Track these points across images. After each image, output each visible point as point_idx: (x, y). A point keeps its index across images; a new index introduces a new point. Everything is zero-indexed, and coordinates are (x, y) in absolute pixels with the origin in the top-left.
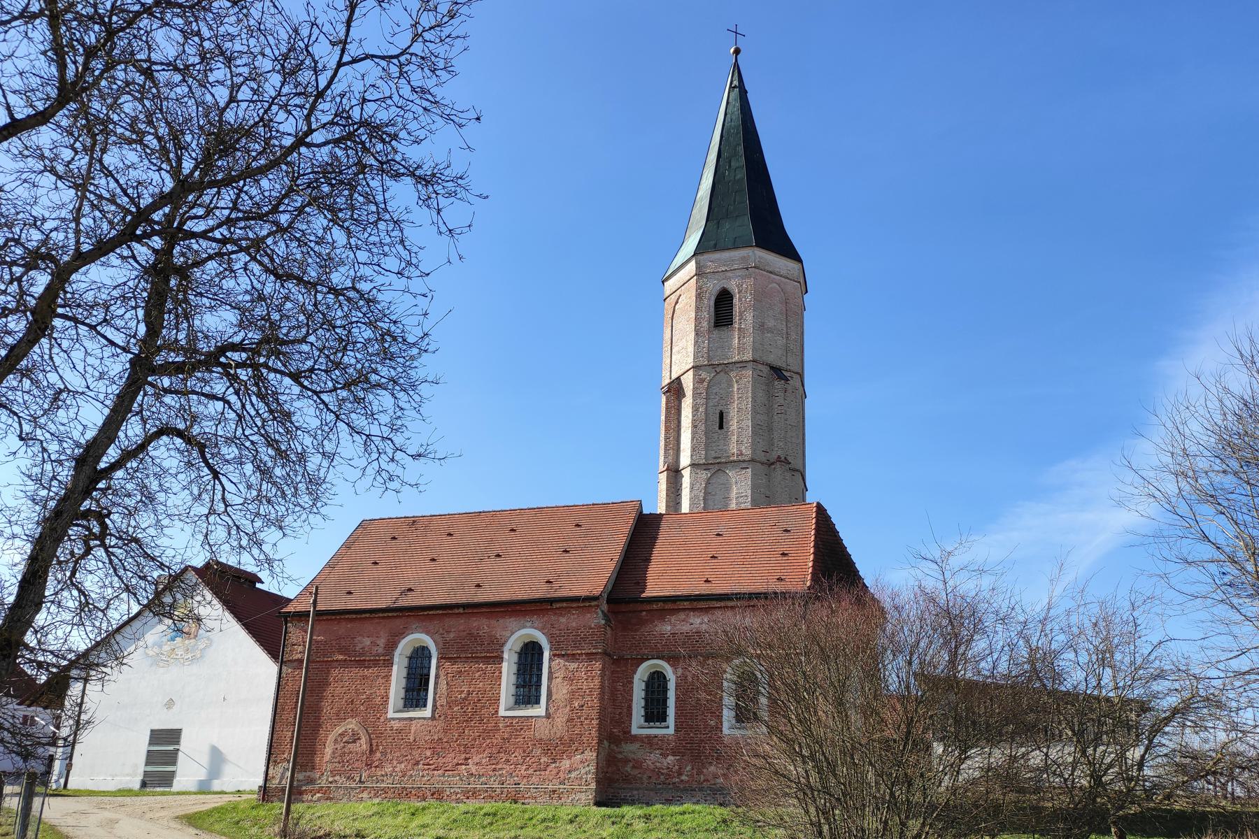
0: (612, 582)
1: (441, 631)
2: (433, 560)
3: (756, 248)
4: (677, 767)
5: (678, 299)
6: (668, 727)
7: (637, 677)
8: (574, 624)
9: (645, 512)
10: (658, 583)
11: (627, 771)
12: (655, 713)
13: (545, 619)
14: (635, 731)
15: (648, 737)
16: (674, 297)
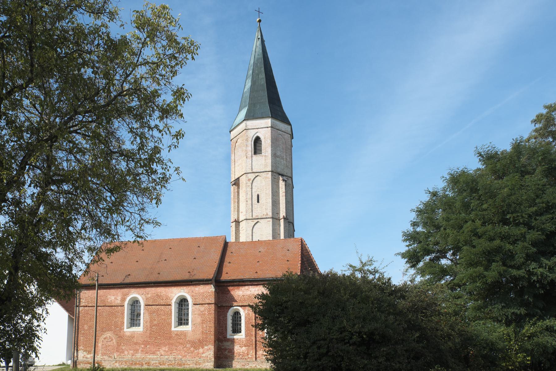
4: (247, 352)
8: (202, 291)
11: (226, 354)
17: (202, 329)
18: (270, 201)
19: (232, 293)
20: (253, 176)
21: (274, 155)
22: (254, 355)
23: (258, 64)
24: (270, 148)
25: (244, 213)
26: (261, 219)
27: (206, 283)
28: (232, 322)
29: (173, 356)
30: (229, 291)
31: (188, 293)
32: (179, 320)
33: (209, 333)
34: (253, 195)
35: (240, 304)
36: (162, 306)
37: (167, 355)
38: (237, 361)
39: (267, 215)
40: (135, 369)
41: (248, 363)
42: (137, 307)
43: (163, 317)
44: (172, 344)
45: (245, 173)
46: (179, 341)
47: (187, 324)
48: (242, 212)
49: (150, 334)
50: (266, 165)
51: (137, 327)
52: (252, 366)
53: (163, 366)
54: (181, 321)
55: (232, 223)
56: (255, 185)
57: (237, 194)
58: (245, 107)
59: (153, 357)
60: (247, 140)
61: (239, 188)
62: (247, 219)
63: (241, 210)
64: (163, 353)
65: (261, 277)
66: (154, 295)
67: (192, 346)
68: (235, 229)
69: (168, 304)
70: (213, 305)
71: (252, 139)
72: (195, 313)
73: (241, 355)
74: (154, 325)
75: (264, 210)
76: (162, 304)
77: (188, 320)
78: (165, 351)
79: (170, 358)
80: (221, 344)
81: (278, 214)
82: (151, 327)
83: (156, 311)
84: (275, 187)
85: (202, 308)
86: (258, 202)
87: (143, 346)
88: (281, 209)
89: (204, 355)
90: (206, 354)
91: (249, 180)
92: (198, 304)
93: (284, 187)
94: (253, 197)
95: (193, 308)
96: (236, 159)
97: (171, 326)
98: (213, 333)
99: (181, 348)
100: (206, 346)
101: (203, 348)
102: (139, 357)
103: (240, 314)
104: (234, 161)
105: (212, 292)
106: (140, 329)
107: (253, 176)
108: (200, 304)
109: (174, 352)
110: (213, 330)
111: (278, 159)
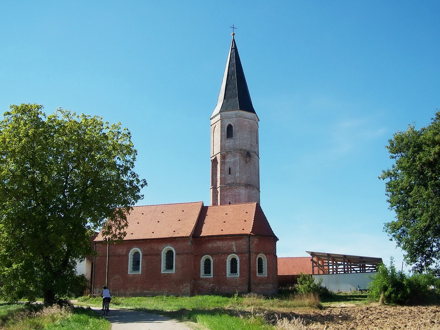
0: (194, 231)
1: (143, 247)
3: (240, 111)
5: (215, 126)
6: (211, 275)
7: (202, 260)
9: (204, 206)
10: (205, 232)
12: (207, 271)
14: (201, 277)
15: (206, 278)
16: (214, 126)
101: (182, 285)
102: (138, 292)
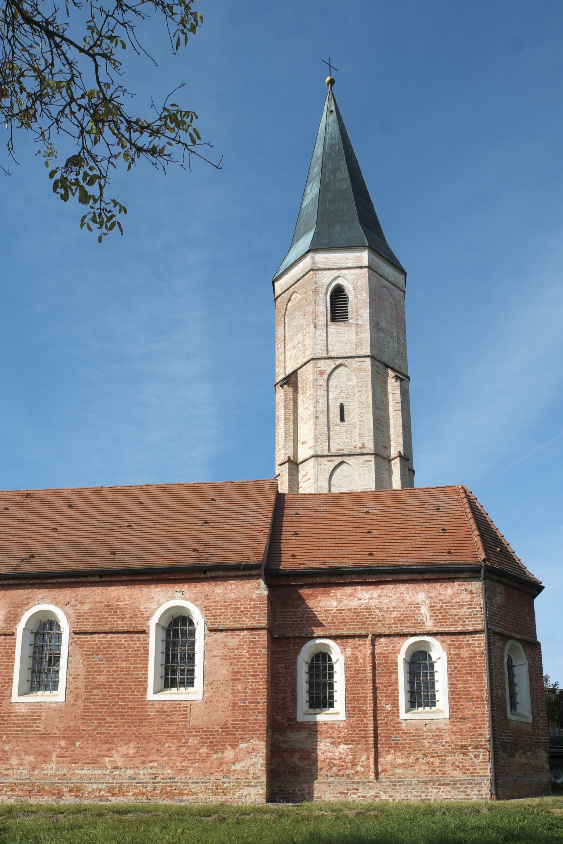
2: (55, 529)
4: (351, 757)
8: (232, 596)
11: (294, 763)
13: (197, 589)
17: (231, 697)
18: (369, 417)
19: (310, 603)
20: (331, 364)
21: (375, 326)
22: (372, 767)
23: (333, 155)
24: (368, 308)
25: (311, 443)
26: (349, 455)
27: (245, 576)
28: (307, 680)
29: (150, 771)
30: (301, 599)
31: (194, 601)
32: (167, 674)
33: (252, 706)
34: (330, 404)
35: (333, 632)
36: (122, 636)
37: (131, 768)
38: (324, 783)
39: (363, 447)
40: (39, 806)
41: (355, 786)
42: (51, 638)
43: (123, 665)
44: (147, 738)
45: (313, 359)
46: (166, 728)
47: (191, 683)
48: (304, 443)
49: (86, 709)
50: (359, 344)
51: (47, 693)
52: (368, 795)
53: (121, 798)
54: (173, 674)
55: (280, 465)
56: (334, 384)
57: (292, 404)
58: (307, 231)
59: (90, 772)
60: (316, 291)
61: (296, 391)
62: (316, 456)
63: (301, 438)
64: (120, 762)
65: (387, 565)
66: (99, 605)
67: (202, 744)
68: (290, 479)
69: (139, 628)
70: (265, 632)
71: (326, 294)
72: (214, 653)
73: (334, 765)
74: (98, 687)
75: (357, 437)
76: (120, 629)
77: (192, 672)
78: (126, 756)
79: (141, 776)
80: (279, 737)
81: (387, 447)
82: (88, 690)
83: (104, 648)
84: (379, 391)
85: (233, 640)
86: (342, 419)
87: (63, 743)
88: (392, 438)
89: (238, 767)
90: (243, 764)
91: (322, 373)
92: (221, 631)
93: (398, 392)
94: (331, 408)
95: (209, 640)
96: (286, 334)
97: (146, 688)
98: (262, 705)
99: (173, 748)
100: (244, 742)
101: (234, 746)
102: (50, 772)
103: (330, 659)
104: (283, 339)
105: (260, 596)
106: (55, 695)
107: (331, 364)
108: (226, 630)
109: (151, 758)
110: (262, 698)
111: (382, 335)
